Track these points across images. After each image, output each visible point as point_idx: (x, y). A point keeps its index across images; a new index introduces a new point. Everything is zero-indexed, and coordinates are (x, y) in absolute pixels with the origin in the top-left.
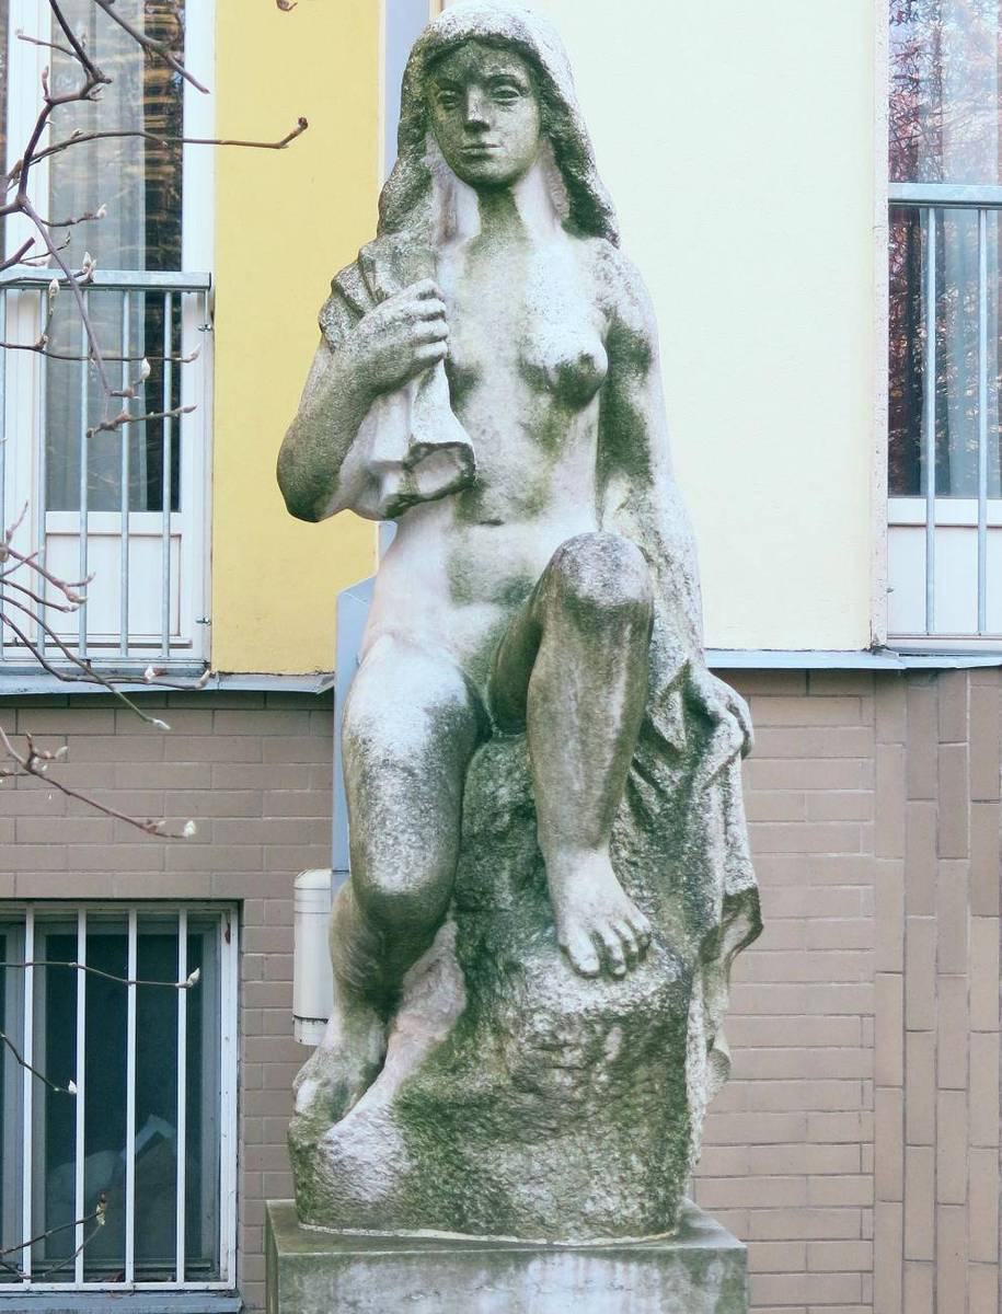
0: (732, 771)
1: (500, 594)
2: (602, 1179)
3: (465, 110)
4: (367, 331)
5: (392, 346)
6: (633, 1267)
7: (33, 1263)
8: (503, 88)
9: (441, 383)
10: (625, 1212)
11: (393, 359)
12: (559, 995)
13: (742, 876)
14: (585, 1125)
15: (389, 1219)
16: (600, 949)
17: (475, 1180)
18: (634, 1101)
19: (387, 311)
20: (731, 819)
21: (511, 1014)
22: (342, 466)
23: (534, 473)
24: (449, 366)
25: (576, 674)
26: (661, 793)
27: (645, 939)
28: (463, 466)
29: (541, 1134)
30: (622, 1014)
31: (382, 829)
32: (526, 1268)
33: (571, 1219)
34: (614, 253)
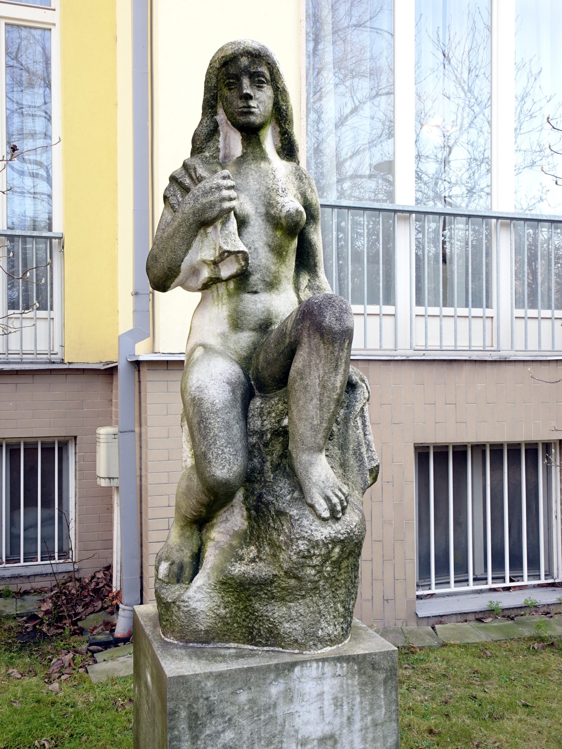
0: (365, 410)
1: (257, 327)
3: (240, 87)
4: (198, 194)
5: (211, 201)
7: (6, 557)
9: (233, 224)
10: (336, 633)
11: (211, 208)
12: (311, 531)
14: (318, 592)
15: (213, 639)
16: (329, 505)
17: (260, 620)
20: (367, 433)
22: (182, 263)
28: (243, 263)
29: (296, 598)
31: (215, 445)
32: (293, 671)
33: (311, 640)
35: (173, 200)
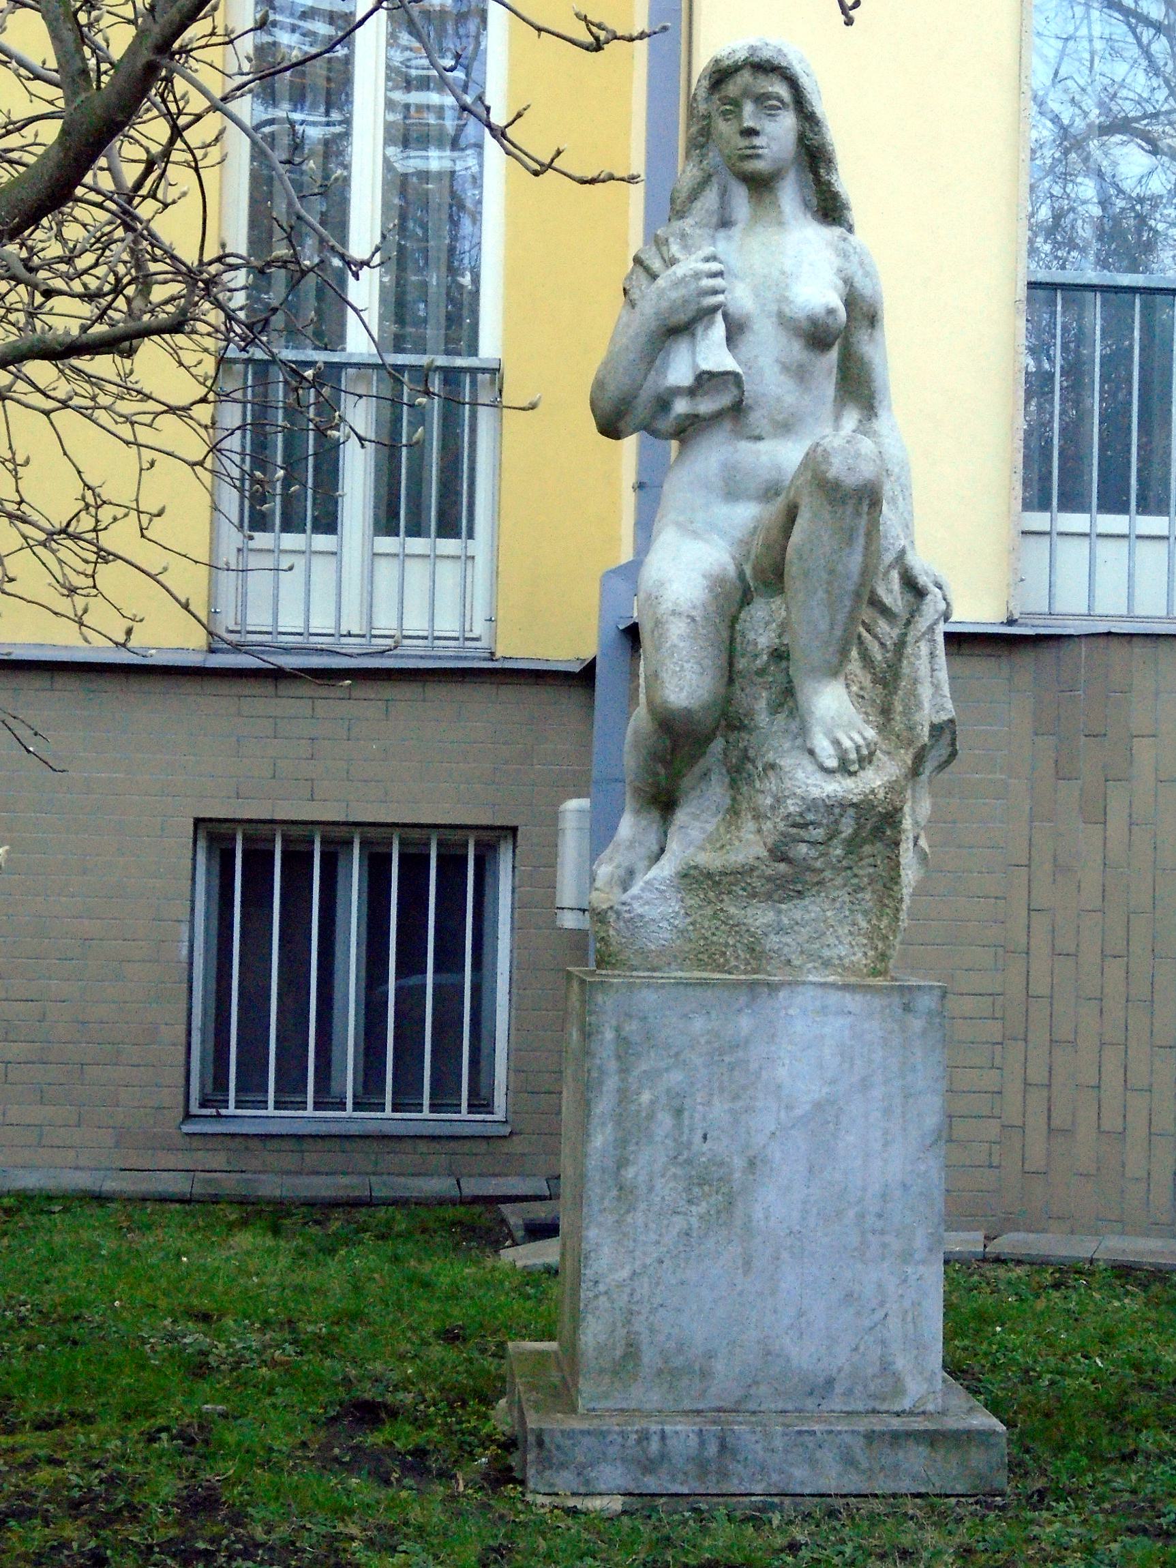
2: (835, 931)
3: (739, 117)
6: (858, 997)
7: (355, 1096)
8: (771, 102)
9: (719, 330)
10: (853, 958)
13: (944, 709)
18: (861, 872)
19: (680, 270)
20: (936, 667)
21: (769, 801)
23: (789, 399)
24: (726, 316)
25: (825, 538)
26: (882, 645)
27: (872, 747)
30: (855, 801)
34: (851, 237)
35: (635, 294)
